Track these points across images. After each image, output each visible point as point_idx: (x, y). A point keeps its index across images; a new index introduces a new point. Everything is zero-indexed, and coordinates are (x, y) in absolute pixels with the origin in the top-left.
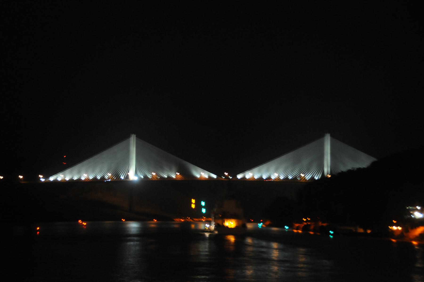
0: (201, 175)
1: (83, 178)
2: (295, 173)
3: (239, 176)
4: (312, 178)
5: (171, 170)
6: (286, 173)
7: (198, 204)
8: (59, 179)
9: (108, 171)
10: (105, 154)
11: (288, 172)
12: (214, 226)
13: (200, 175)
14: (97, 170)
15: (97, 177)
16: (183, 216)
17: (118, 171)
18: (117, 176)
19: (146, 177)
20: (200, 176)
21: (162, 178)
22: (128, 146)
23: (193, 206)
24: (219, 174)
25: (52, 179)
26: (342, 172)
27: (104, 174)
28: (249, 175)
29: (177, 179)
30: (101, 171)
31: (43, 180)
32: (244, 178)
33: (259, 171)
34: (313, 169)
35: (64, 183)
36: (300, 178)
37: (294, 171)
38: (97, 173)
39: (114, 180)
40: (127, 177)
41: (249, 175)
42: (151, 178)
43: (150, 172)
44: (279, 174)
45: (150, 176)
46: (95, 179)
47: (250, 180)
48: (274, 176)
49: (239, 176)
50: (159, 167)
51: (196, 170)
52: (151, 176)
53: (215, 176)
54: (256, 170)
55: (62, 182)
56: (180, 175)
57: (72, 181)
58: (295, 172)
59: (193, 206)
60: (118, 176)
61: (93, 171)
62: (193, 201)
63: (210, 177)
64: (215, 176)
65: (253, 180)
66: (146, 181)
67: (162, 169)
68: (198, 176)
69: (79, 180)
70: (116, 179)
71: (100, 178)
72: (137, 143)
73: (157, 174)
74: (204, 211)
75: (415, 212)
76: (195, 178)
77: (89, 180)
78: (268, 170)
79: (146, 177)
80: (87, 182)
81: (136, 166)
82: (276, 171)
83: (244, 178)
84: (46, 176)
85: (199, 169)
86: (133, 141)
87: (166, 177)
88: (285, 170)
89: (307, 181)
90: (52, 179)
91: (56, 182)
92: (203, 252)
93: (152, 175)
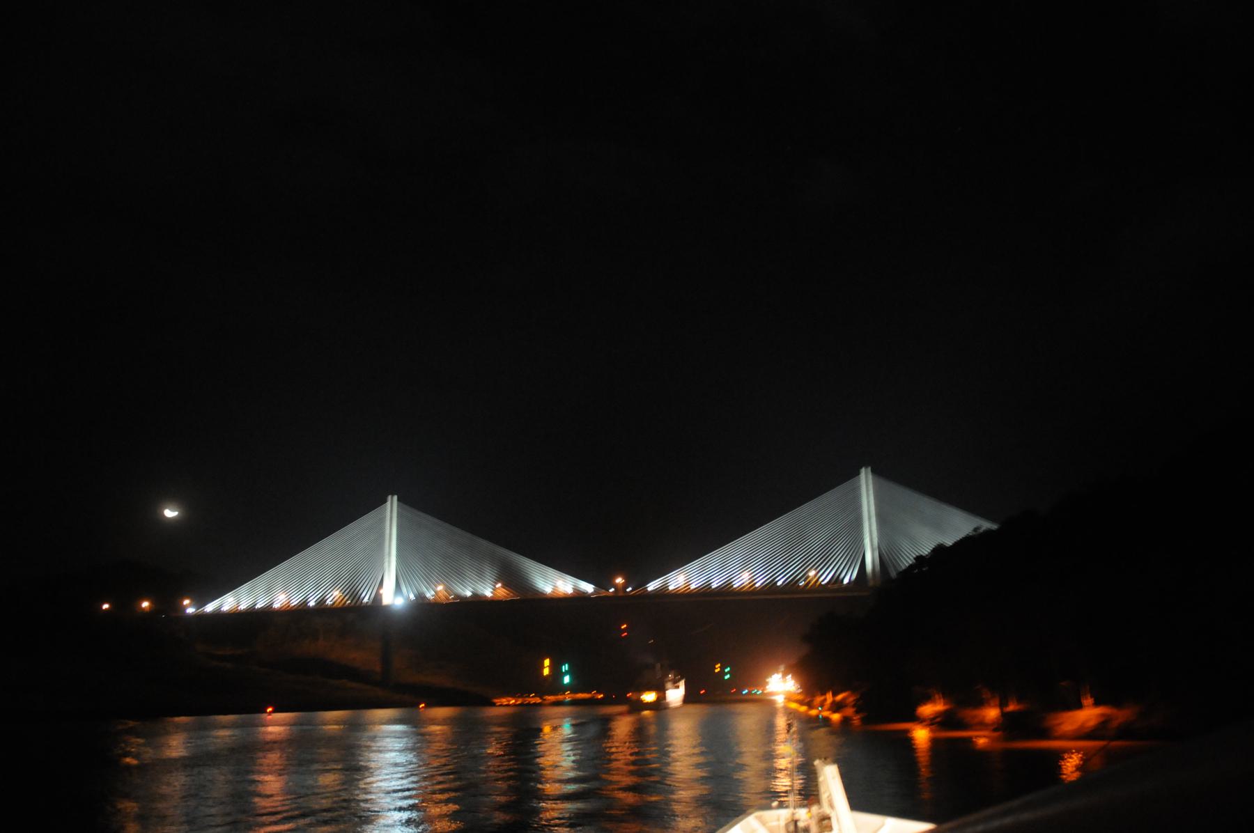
1: (276, 606)
3: (652, 586)
4: (837, 580)
5: (481, 575)
7: (555, 667)
8: (225, 608)
9: (334, 585)
13: (554, 586)
19: (421, 597)
20: (472, 592)
21: (458, 596)
22: (382, 521)
23: (546, 672)
25: (210, 608)
26: (922, 556)
28: (678, 580)
29: (497, 598)
30: (317, 586)
31: (190, 610)
32: (662, 593)
36: (805, 581)
39: (345, 606)
40: (378, 598)
41: (678, 580)
42: (432, 598)
43: (429, 582)
45: (430, 595)
48: (742, 579)
49: (652, 586)
50: (453, 571)
51: (545, 577)
52: (433, 593)
53: (588, 588)
54: (694, 566)
56: (502, 587)
57: (705, 594)
59: (546, 672)
60: (355, 595)
61: (300, 587)
62: (547, 662)
63: (576, 590)
64: (588, 588)
66: (422, 607)
67: (460, 575)
68: (548, 589)
69: (726, 591)
70: (350, 603)
72: (400, 516)
73: (447, 589)
79: (421, 597)
82: (745, 565)
84: (201, 601)
85: (551, 572)
86: (392, 506)
87: (469, 594)
89: (363, 605)
90: (210, 608)
91: (218, 616)
93: (435, 591)
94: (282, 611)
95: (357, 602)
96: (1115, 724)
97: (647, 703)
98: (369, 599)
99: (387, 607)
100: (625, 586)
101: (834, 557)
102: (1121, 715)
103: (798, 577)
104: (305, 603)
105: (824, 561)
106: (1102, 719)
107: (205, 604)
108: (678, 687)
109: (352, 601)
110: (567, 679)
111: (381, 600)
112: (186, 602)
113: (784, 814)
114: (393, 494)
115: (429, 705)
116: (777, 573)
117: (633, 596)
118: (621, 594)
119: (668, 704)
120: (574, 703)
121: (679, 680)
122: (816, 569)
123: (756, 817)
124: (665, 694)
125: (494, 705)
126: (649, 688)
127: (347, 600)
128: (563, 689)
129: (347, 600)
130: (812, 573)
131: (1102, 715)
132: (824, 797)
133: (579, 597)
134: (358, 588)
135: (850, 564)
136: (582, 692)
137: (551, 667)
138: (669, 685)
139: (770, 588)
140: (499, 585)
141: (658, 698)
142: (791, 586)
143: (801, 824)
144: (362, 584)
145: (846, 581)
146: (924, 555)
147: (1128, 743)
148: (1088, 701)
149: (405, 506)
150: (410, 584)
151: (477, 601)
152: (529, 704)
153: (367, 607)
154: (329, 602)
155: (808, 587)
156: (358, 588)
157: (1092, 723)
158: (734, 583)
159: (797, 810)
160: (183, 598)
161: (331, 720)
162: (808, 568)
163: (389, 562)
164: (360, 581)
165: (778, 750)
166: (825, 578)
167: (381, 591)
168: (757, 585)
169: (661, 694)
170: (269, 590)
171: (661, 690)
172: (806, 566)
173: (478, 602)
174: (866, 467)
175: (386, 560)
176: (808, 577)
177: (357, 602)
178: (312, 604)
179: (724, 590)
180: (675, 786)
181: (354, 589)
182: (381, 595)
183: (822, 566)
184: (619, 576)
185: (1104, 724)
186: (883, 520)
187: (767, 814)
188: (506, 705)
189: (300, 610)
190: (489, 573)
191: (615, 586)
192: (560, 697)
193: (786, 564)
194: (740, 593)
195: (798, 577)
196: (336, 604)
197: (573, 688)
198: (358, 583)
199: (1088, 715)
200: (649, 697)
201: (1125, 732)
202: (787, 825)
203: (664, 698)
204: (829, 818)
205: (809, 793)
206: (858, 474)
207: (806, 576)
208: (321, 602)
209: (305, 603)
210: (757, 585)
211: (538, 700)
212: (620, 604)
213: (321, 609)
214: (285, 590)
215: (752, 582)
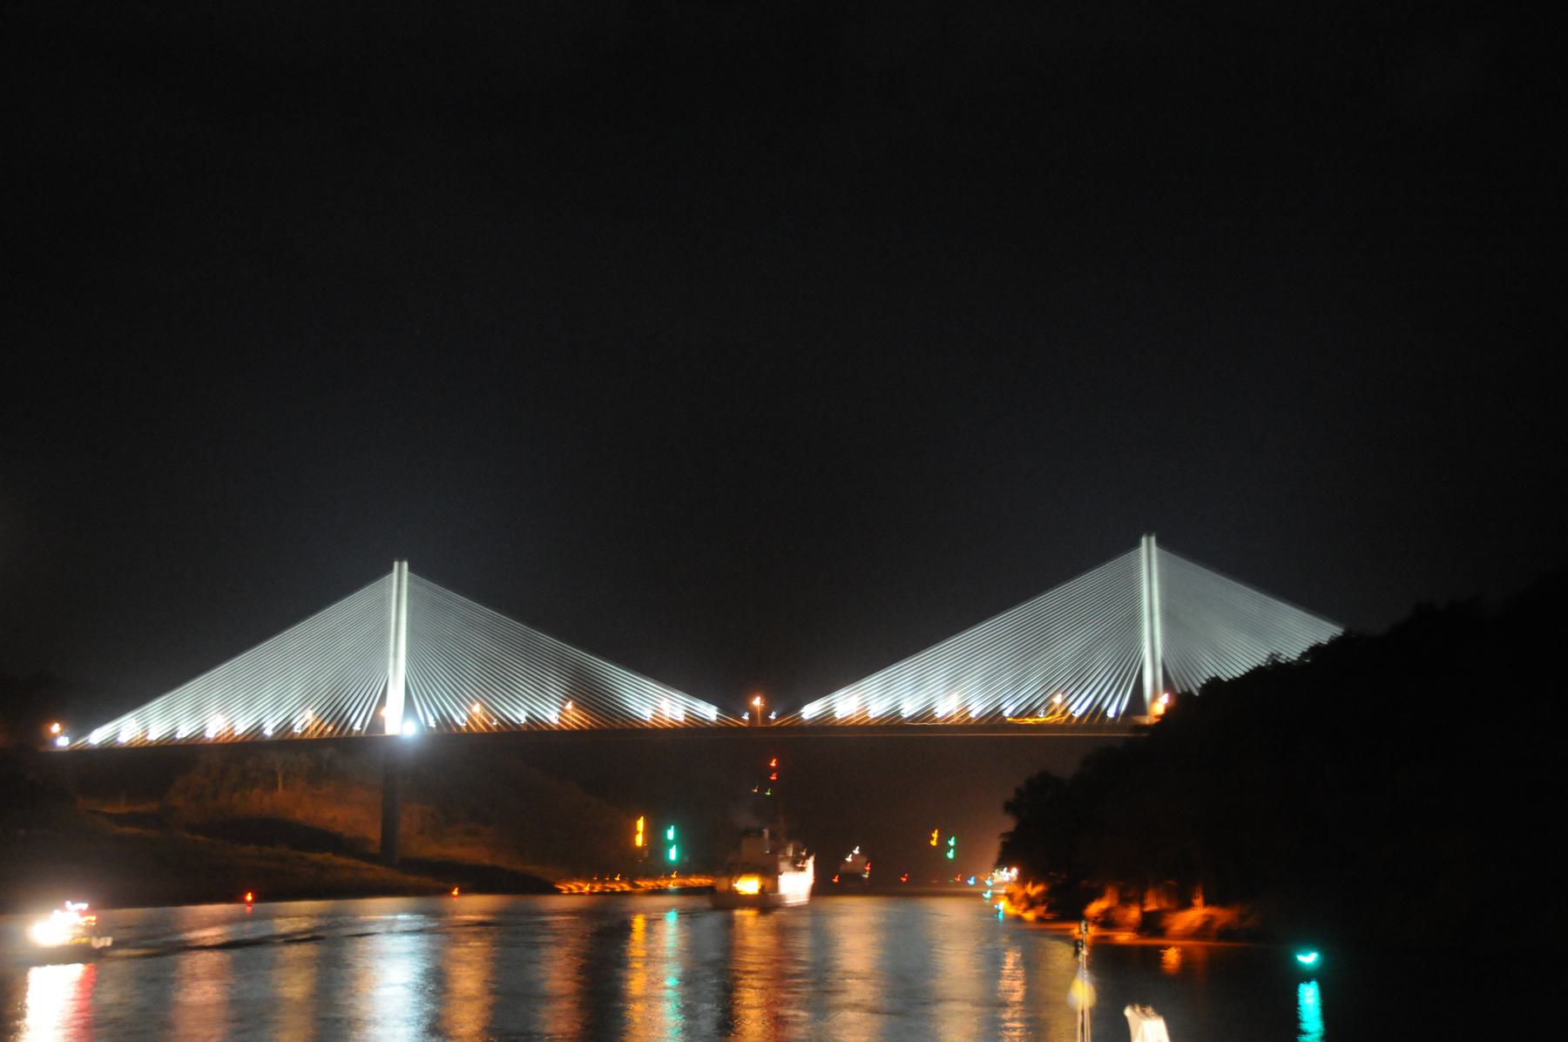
0: (657, 711)
1: (211, 734)
2: (1025, 696)
3: (810, 711)
4: (1096, 712)
5: (542, 691)
6: (462, 693)
7: (655, 833)
9: (305, 702)
11: (478, 690)
12: (634, 926)
15: (292, 728)
16: (602, 871)
17: (343, 706)
19: (445, 723)
22: (383, 603)
23: (639, 840)
24: (729, 701)
25: (97, 737)
31: (63, 742)
32: (826, 727)
38: (182, 713)
40: (376, 724)
43: (459, 698)
45: (461, 719)
47: (163, 743)
48: (947, 707)
49: (810, 711)
50: (496, 681)
51: (642, 694)
53: (709, 712)
54: (872, 683)
58: (497, 692)
59: (639, 840)
60: (339, 717)
64: (709, 712)
65: (143, 745)
74: (673, 854)
75: (1092, 988)
76: (628, 717)
77: (233, 737)
79: (445, 723)
81: (409, 680)
82: (953, 683)
83: (828, 715)
85: (651, 687)
86: (400, 580)
87: (521, 717)
88: (988, 682)
90: (97, 737)
93: (470, 714)
96: (1217, 925)
97: (747, 896)
98: (362, 726)
102: (1223, 916)
104: (258, 729)
105: (1078, 680)
106: (1206, 919)
107: (88, 730)
108: (802, 869)
109: (335, 727)
110: (673, 854)
111: (382, 729)
112: (55, 728)
115: (463, 892)
117: (779, 728)
118: (759, 723)
119: (781, 898)
120: (685, 891)
121: (807, 857)
122: (1063, 693)
124: (776, 880)
125: (558, 892)
126: (748, 870)
128: (665, 870)
130: (1058, 699)
131: (1205, 916)
133: (694, 730)
136: (698, 873)
137: (646, 832)
138: (784, 865)
139: (993, 720)
140: (569, 706)
141: (762, 890)
144: (374, 683)
145: (1111, 714)
146: (1238, 676)
147: (1229, 944)
148: (1198, 901)
149: (420, 579)
152: (613, 892)
154: (297, 730)
157: (1198, 923)
160: (51, 721)
161: (298, 914)
165: (83, 913)
166: (1078, 710)
169: (769, 883)
170: (197, 709)
171: (769, 872)
173: (536, 736)
174: (1149, 535)
175: (391, 659)
176: (1052, 704)
178: (269, 732)
179: (894, 723)
181: (339, 708)
182: (383, 719)
184: (758, 695)
185: (1208, 923)
186: (1171, 618)
188: (574, 894)
189: (247, 743)
190: (555, 686)
192: (662, 883)
193: (1017, 684)
196: (310, 732)
197: (684, 870)
198: (345, 700)
199: (1195, 915)
200: (748, 885)
201: (1226, 933)
203: (775, 888)
206: (1137, 544)
207: (1048, 704)
208: (286, 727)
209: (258, 729)
211: (627, 888)
212: (758, 739)
213: (286, 743)
214: (224, 709)
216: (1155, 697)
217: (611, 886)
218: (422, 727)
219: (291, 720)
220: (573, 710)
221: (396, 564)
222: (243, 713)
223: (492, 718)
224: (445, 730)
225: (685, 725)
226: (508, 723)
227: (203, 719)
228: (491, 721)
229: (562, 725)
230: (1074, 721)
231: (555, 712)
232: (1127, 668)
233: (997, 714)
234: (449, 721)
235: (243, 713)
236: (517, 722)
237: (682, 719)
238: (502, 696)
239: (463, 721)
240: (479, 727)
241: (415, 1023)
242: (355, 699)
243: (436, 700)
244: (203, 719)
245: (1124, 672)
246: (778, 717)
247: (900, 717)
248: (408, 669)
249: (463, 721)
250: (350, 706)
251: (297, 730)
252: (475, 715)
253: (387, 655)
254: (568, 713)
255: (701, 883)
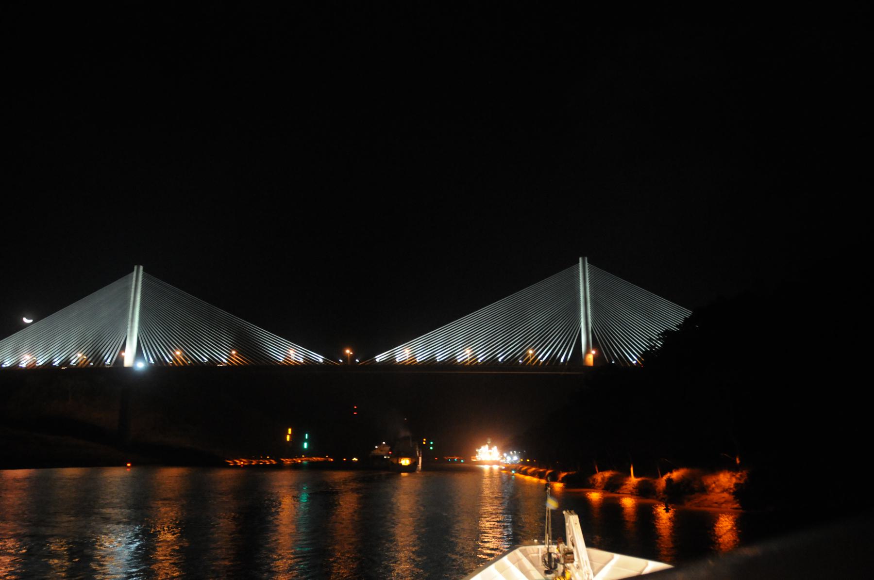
0: (288, 357)
1: (23, 365)
3: (379, 358)
4: (553, 360)
5: (218, 343)
9: (78, 348)
10: (74, 310)
14: (56, 345)
18: (523, 356)
19: (160, 362)
22: (127, 289)
27: (69, 355)
28: (403, 354)
32: (390, 364)
33: (427, 345)
34: (152, 330)
35: (410, 368)
37: (83, 345)
38: (38, 353)
39: (89, 366)
40: (120, 361)
41: (403, 354)
43: (169, 348)
44: (88, 354)
46: (49, 364)
48: (465, 355)
49: (379, 358)
53: (320, 359)
54: (419, 341)
55: (28, 368)
57: (430, 365)
60: (97, 357)
61: (46, 349)
63: (307, 359)
64: (320, 359)
66: (160, 370)
69: (450, 364)
71: (26, 365)
78: (447, 343)
80: (33, 370)
82: (467, 342)
85: (284, 342)
86: (137, 278)
92: (63, 522)
94: (79, 368)
95: (99, 364)
98: (111, 362)
99: (129, 369)
100: (353, 358)
101: (158, 336)
103: (518, 355)
105: (542, 341)
113: (542, 548)
114: (139, 265)
116: (456, 347)
123: (521, 551)
127: (90, 362)
128: (300, 452)
129: (90, 362)
130: (531, 352)
132: (569, 537)
133: (310, 365)
134: (101, 352)
135: (567, 345)
139: (491, 363)
142: (511, 363)
143: (553, 556)
150: (150, 349)
151: (213, 364)
153: (110, 370)
154: (73, 362)
155: (466, 364)
156: (101, 352)
158: (458, 358)
159: (550, 546)
162: (527, 347)
163: (132, 327)
164: (66, 346)
166: (543, 357)
167: (123, 354)
168: (479, 361)
170: (16, 351)
172: (524, 345)
175: (129, 323)
177: (99, 364)
178: (56, 363)
179: (84, 366)
180: (165, 555)
183: (483, 346)
184: (595, 350)
187: (530, 549)
190: (226, 340)
191: (345, 357)
193: (506, 343)
194: (463, 366)
195: (518, 355)
202: (543, 557)
204: (572, 553)
205: (560, 535)
207: (525, 354)
208: (66, 362)
210: (479, 361)
214: (31, 351)
215: (474, 357)
216: (588, 352)
217: (264, 461)
218: (148, 364)
219: (53, 360)
220: (236, 354)
221: (136, 267)
222: (10, 355)
223: (188, 359)
224: (159, 365)
225: (303, 364)
226: (162, 360)
227: (18, 356)
228: (187, 360)
229: (229, 364)
230: (540, 364)
231: (228, 356)
232: (570, 330)
233: (433, 360)
234: (162, 360)
235: (10, 355)
236: (203, 362)
237: (302, 361)
238: (503, 341)
239: (170, 360)
240: (179, 363)
241: (282, 503)
242: (107, 346)
243: (174, 344)
244: (18, 356)
245: (528, 331)
246: (360, 362)
247: (396, 361)
248: (139, 328)
249: (170, 360)
250: (102, 348)
251: (73, 362)
252: (177, 356)
253: (127, 321)
254: (233, 356)
255: (318, 460)
